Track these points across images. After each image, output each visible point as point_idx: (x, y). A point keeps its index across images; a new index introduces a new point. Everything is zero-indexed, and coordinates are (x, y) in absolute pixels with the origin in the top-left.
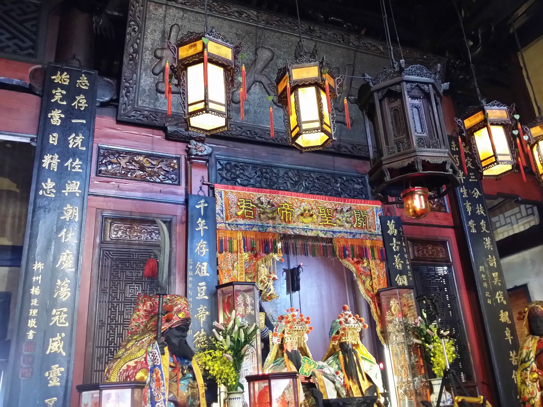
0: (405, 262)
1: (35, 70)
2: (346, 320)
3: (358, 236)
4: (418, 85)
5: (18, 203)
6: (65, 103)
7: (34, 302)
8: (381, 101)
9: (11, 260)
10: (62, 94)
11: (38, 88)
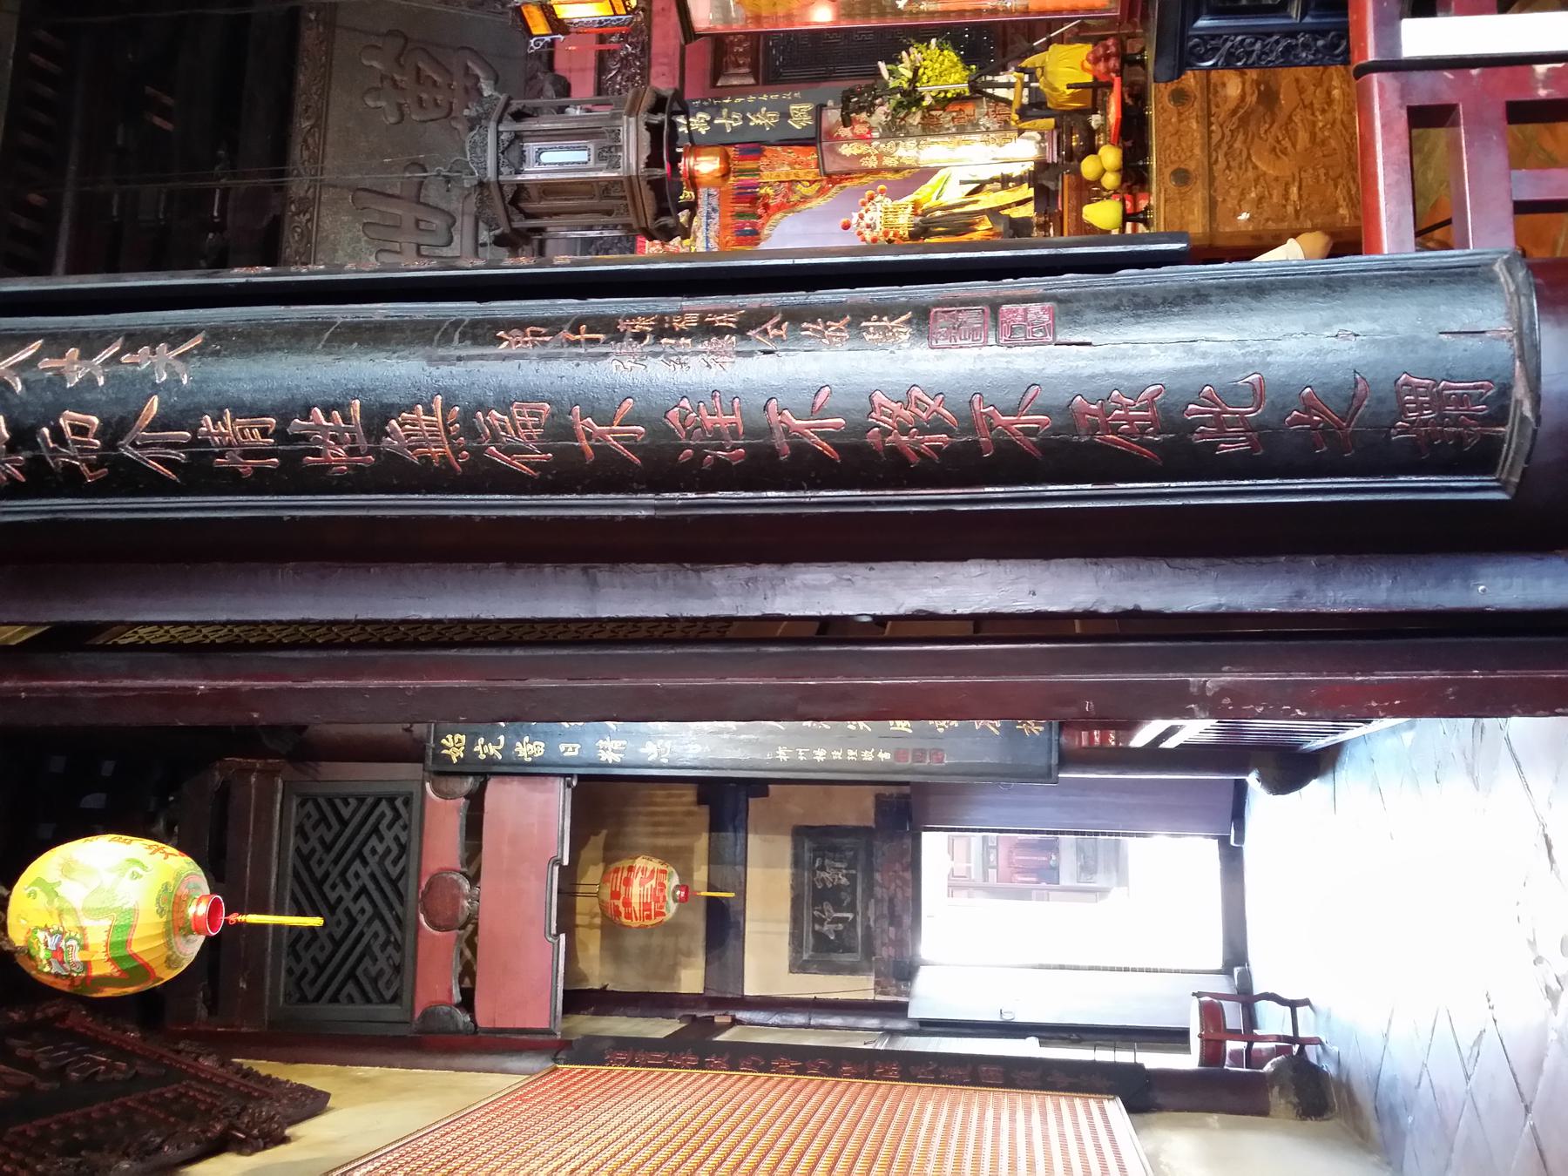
0: (764, 103)
1: (436, 791)
2: (868, 226)
3: (715, 202)
4: (502, 150)
5: (628, 829)
6: (502, 738)
7: (837, 755)
8: (529, 216)
9: (735, 830)
10: (486, 743)
11: (468, 784)
